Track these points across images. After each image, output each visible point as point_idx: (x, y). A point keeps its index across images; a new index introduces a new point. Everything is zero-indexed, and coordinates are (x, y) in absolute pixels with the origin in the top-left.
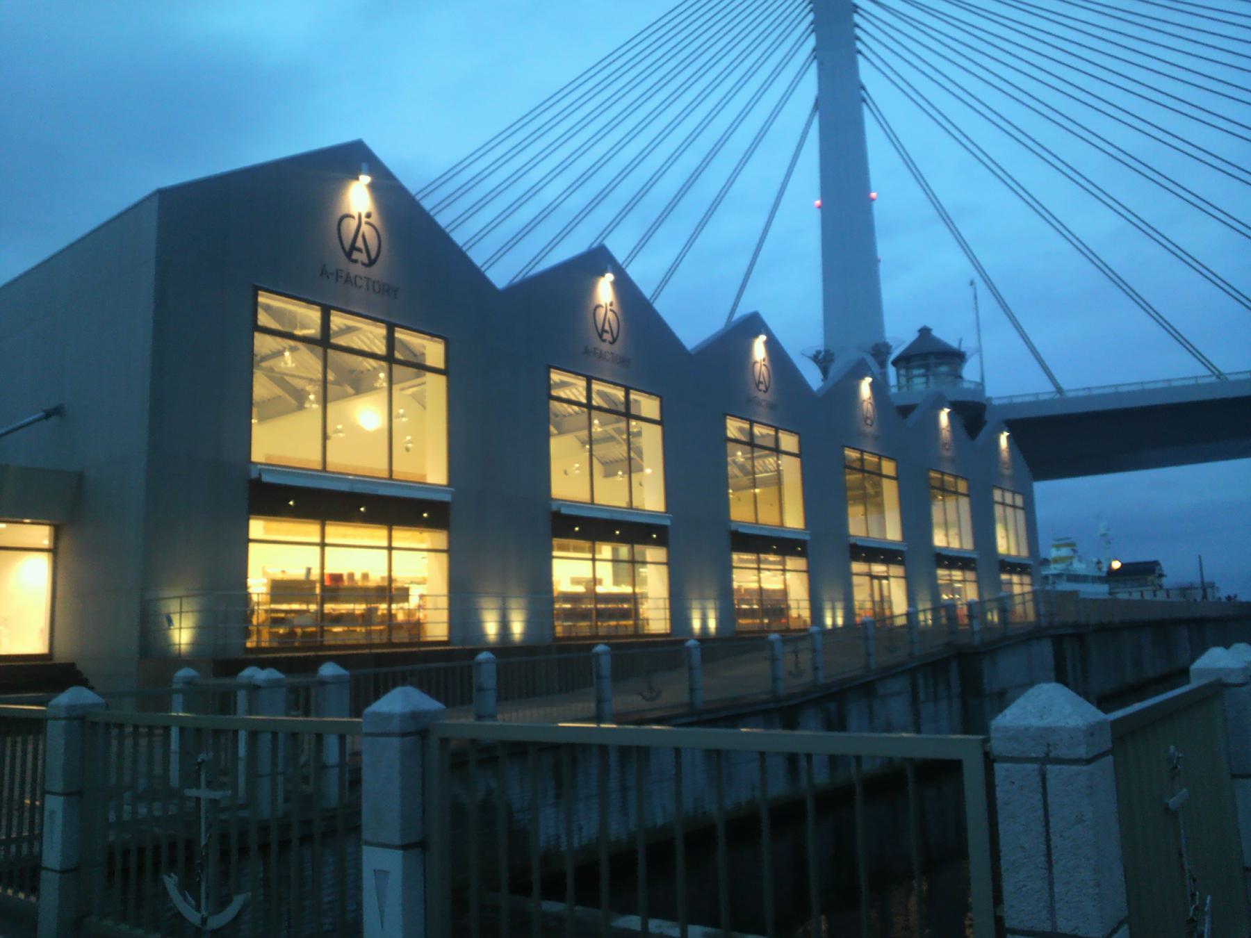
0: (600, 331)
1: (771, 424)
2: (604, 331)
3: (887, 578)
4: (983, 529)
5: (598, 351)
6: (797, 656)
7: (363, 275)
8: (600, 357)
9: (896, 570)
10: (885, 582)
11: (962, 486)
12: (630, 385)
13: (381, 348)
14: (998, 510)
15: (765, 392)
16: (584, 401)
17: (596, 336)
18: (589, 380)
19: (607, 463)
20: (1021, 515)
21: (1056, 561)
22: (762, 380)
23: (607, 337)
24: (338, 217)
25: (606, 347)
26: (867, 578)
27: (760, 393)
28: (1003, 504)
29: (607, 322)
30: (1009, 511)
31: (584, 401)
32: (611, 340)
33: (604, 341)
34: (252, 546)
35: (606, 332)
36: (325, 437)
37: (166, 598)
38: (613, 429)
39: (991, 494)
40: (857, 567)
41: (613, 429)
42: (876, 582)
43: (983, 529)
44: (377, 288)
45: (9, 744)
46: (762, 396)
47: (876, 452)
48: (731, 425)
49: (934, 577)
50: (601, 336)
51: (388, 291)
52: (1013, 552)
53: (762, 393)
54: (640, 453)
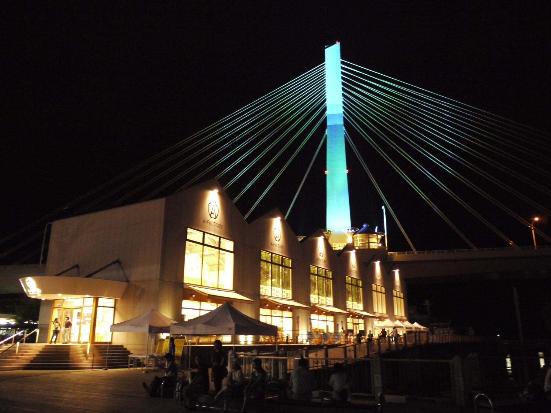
0: (210, 213)
3: (358, 324)
5: (208, 221)
6: (148, 348)
7: (278, 244)
8: (275, 246)
10: (357, 325)
16: (270, 261)
19: (211, 265)
25: (212, 220)
26: (352, 324)
27: (211, 218)
28: (397, 297)
30: (399, 299)
33: (212, 217)
34: (182, 309)
35: (213, 214)
38: (215, 252)
41: (215, 252)
42: (355, 325)
44: (217, 225)
46: (277, 243)
49: (346, 320)
51: (220, 226)
53: (213, 218)
54: (224, 261)
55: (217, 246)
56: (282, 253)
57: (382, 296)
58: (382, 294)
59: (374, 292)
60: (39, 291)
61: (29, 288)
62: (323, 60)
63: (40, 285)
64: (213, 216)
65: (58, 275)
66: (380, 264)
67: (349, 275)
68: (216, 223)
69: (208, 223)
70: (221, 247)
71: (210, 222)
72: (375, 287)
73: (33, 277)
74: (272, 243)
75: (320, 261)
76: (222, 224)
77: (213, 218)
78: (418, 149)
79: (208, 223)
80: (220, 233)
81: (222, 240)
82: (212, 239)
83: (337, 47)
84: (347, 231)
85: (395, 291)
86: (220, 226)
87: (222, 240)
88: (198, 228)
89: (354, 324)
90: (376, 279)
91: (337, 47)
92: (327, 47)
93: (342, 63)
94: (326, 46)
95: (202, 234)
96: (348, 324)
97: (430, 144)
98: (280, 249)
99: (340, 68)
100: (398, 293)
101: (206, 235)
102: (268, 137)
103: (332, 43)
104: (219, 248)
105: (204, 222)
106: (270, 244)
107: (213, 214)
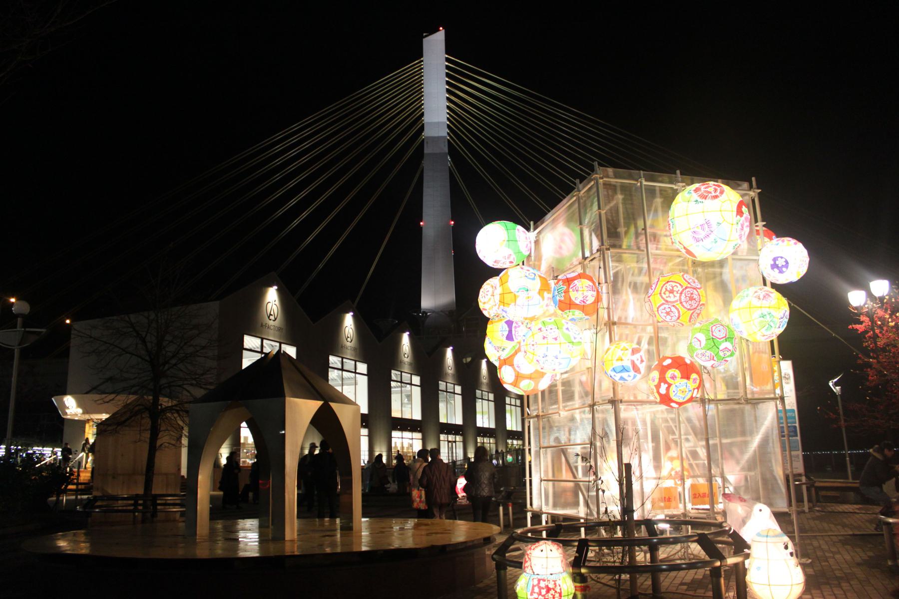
0: (269, 315)
1: (287, 343)
2: (271, 315)
4: (469, 410)
5: (267, 325)
9: (458, 438)
11: (491, 396)
12: (282, 341)
13: (340, 366)
14: (508, 407)
15: (274, 321)
17: (267, 317)
18: (262, 339)
20: (519, 409)
21: (648, 446)
22: (349, 336)
23: (349, 340)
24: (268, 301)
25: (271, 323)
27: (270, 321)
29: (272, 311)
30: (513, 408)
31: (354, 371)
32: (274, 319)
33: (271, 320)
35: (272, 315)
36: (483, 423)
37: (417, 470)
39: (438, 385)
40: (442, 437)
42: (450, 444)
43: (469, 410)
45: (250, 544)
46: (349, 344)
47: (452, 382)
48: (266, 343)
50: (269, 317)
52: (514, 429)
53: (272, 321)
55: (399, 380)
56: (280, 339)
57: (517, 410)
58: (517, 407)
59: (507, 406)
60: (80, 411)
61: (68, 408)
62: (421, 55)
63: (80, 404)
64: (272, 318)
65: (87, 393)
66: (453, 350)
67: (398, 368)
68: (276, 325)
69: (267, 327)
70: (345, 368)
71: (269, 326)
72: (480, 395)
73: (74, 395)
74: (342, 345)
75: (405, 363)
76: (282, 327)
77: (272, 321)
78: (371, 103)
79: (267, 327)
80: (355, 357)
81: (357, 363)
82: (271, 344)
83: (439, 37)
84: (535, 345)
85: (480, 390)
86: (280, 329)
87: (357, 363)
88: (268, 337)
89: (449, 442)
90: (482, 383)
91: (439, 37)
92: (426, 36)
93: (447, 60)
94: (424, 34)
95: (445, 383)
96: (441, 442)
97: (482, 125)
98: (276, 332)
99: (445, 67)
100: (450, 386)
101: (265, 341)
102: (289, 142)
103: (434, 30)
104: (355, 373)
105: (262, 325)
106: (358, 350)
107: (272, 315)
